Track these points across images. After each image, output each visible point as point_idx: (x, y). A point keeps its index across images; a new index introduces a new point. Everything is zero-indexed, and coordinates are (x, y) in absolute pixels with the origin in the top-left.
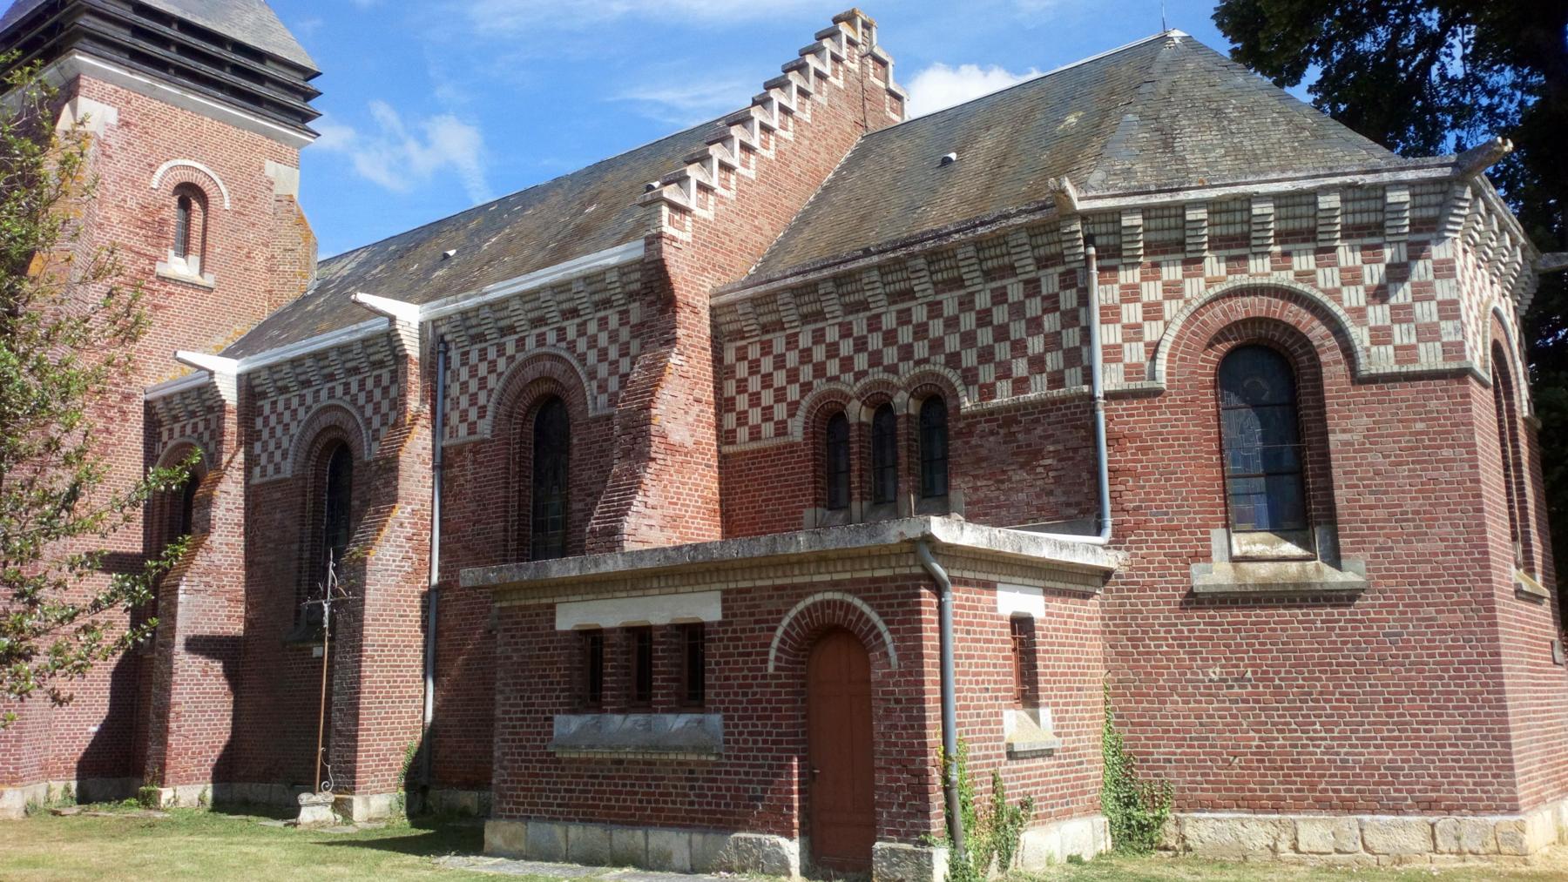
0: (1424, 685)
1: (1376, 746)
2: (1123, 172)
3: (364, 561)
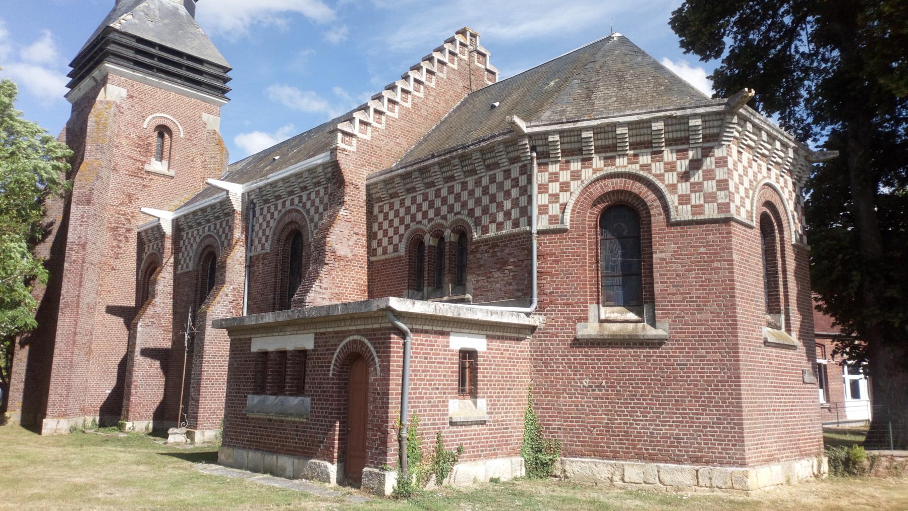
0: (697, 393)
1: (669, 426)
2: (560, 111)
3: (205, 313)
